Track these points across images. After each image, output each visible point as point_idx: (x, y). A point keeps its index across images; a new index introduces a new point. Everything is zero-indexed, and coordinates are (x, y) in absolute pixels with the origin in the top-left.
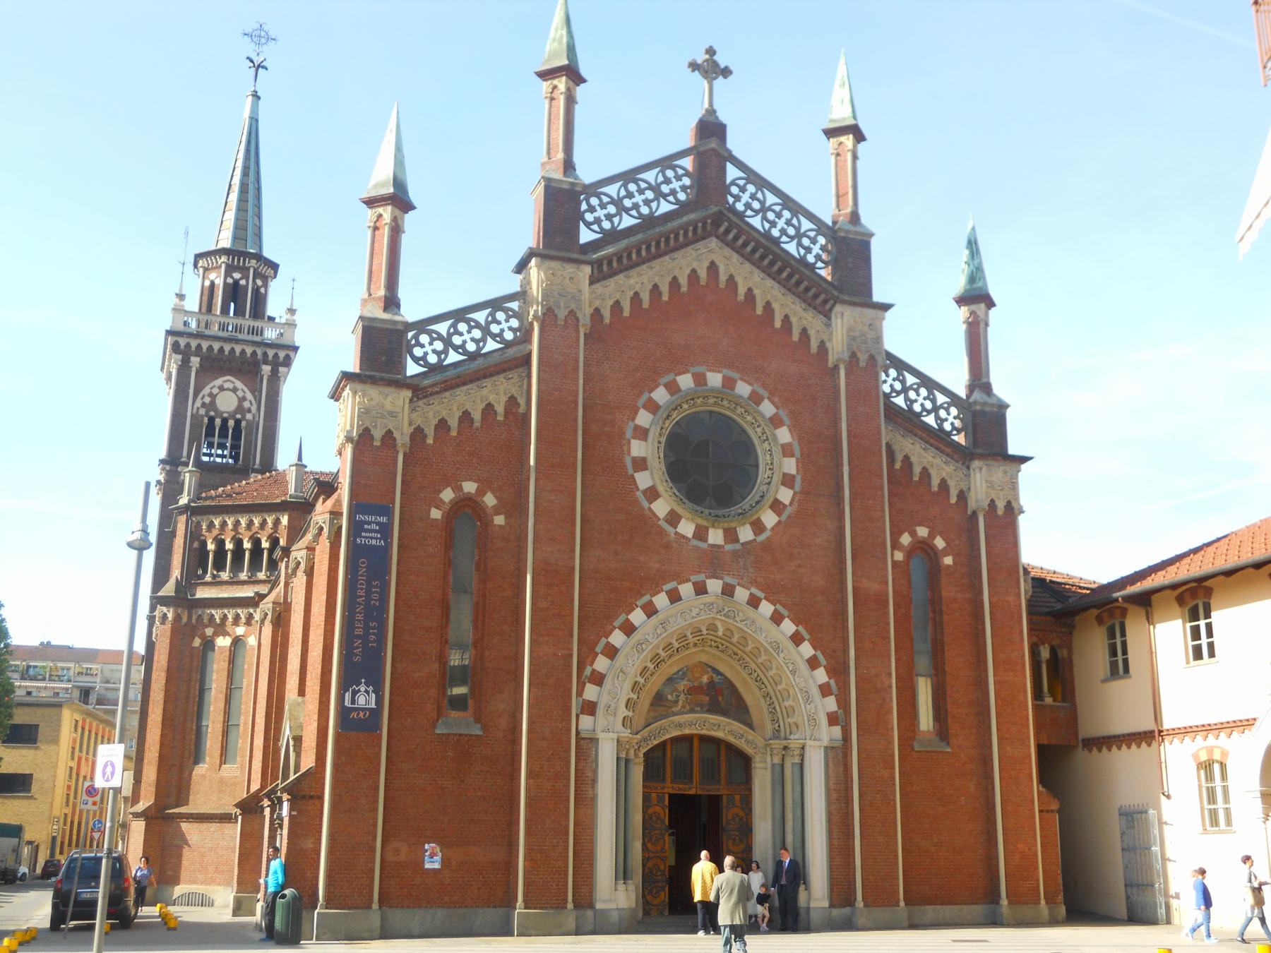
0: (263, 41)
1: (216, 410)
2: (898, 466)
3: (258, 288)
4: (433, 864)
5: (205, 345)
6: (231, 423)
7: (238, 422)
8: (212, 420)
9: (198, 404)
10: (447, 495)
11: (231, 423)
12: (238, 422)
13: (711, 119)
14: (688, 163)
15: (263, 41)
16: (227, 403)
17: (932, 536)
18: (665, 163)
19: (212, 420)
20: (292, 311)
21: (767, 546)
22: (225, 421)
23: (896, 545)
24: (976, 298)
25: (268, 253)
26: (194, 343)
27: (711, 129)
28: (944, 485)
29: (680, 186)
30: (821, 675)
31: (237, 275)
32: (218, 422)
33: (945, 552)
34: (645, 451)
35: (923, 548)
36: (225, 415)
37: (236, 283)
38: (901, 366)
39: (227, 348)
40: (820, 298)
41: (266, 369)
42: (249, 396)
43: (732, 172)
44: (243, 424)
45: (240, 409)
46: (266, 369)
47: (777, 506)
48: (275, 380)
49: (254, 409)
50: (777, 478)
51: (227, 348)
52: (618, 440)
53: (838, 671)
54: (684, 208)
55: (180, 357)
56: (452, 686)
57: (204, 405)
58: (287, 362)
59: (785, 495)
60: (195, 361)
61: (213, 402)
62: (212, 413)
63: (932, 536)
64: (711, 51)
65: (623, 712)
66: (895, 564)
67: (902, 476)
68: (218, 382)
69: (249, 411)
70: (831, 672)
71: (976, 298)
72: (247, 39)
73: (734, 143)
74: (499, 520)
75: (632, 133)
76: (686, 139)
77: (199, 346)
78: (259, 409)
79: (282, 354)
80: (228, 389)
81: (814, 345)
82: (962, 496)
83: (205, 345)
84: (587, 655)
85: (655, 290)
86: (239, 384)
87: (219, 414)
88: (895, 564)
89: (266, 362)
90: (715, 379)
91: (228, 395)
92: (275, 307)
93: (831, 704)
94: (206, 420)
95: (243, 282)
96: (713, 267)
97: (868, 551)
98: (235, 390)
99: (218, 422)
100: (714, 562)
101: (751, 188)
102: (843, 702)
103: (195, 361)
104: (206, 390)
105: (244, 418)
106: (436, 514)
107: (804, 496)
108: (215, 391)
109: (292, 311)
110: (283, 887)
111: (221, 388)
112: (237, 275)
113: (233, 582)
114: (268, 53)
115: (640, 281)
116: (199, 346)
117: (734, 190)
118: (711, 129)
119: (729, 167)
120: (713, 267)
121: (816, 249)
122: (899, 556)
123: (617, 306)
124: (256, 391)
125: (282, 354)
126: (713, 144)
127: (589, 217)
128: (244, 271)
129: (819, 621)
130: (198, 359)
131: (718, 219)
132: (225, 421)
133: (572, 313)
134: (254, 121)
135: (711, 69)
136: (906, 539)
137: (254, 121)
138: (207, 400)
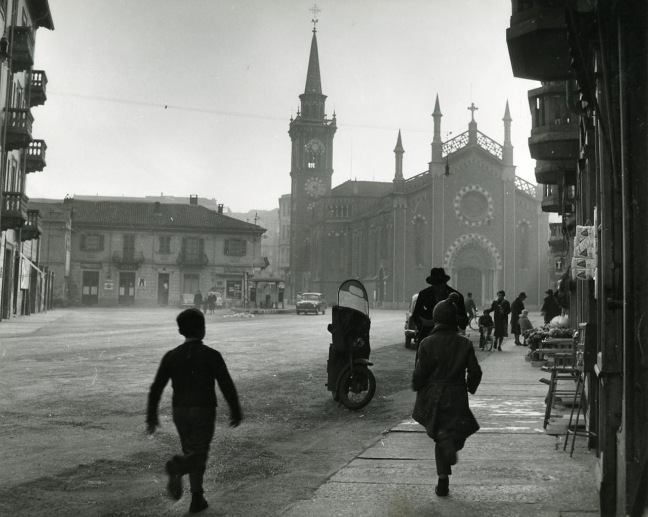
7: (319, 154)
14: (467, 134)
27: (473, 126)
29: (466, 140)
38: (520, 179)
43: (479, 135)
54: (467, 145)
56: (536, 428)
61: (311, 148)
64: (473, 104)
68: (312, 141)
72: (311, 11)
73: (479, 128)
75: (454, 129)
76: (466, 128)
84: (445, 252)
87: (313, 151)
90: (474, 224)
98: (317, 143)
101: (483, 138)
102: (503, 260)
109: (334, 115)
111: (313, 143)
114: (319, 16)
117: (479, 139)
118: (473, 126)
119: (478, 133)
121: (499, 152)
122: (518, 226)
127: (445, 150)
135: (473, 108)
136: (520, 222)
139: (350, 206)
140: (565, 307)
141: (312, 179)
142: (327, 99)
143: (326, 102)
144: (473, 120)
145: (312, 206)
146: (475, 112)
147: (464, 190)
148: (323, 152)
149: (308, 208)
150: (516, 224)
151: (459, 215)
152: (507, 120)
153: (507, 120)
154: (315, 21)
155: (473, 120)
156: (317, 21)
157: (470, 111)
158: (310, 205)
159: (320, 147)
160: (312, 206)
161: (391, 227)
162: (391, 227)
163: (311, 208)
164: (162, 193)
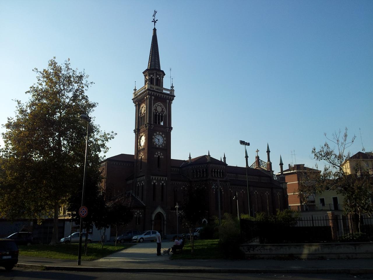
3: (158, 78)
24: (268, 152)
25: (161, 69)
31: (151, 76)
36: (159, 112)
37: (152, 77)
44: (163, 115)
45: (162, 111)
46: (168, 101)
48: (170, 104)
60: (153, 97)
62: (156, 112)
68: (157, 104)
71: (268, 152)
78: (166, 110)
80: (159, 106)
86: (162, 105)
91: (159, 107)
95: (153, 77)
98: (161, 106)
99: (158, 114)
108: (157, 106)
110: (276, 175)
111: (158, 105)
112: (151, 76)
130: (154, 97)
134: (155, 25)
137: (155, 25)
138: (155, 108)
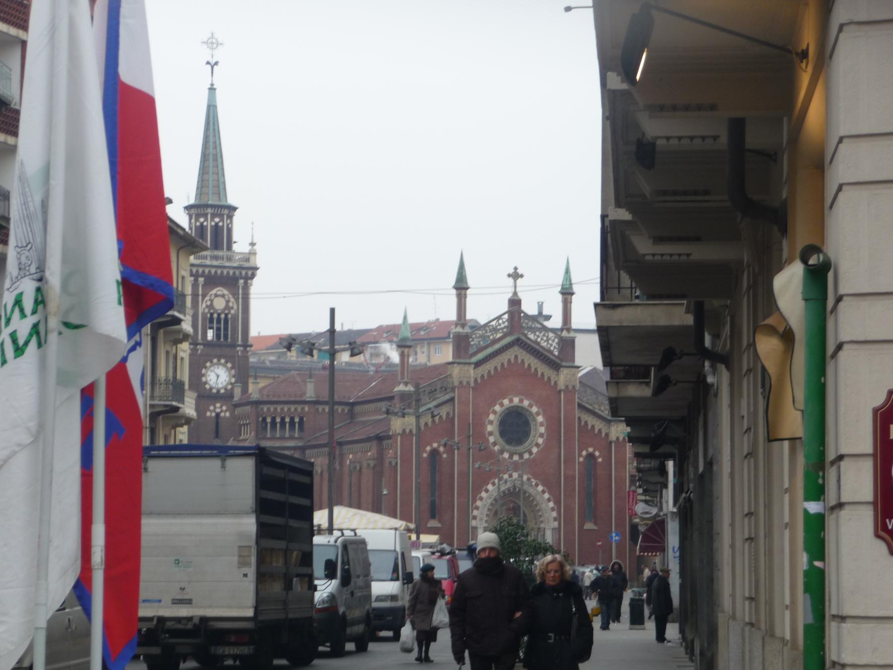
0: (215, 46)
1: (214, 308)
2: (583, 423)
4: (512, 560)
5: (207, 271)
6: (223, 316)
7: (226, 315)
8: (212, 315)
9: (204, 306)
10: (428, 448)
11: (223, 316)
12: (226, 315)
13: (516, 298)
14: (506, 316)
15: (215, 46)
16: (219, 304)
17: (594, 451)
18: (499, 318)
19: (212, 315)
20: (253, 244)
21: (534, 460)
22: (219, 315)
23: (580, 455)
26: (200, 270)
28: (600, 431)
30: (551, 504)
32: (215, 316)
33: (599, 457)
34: (492, 428)
35: (591, 456)
39: (219, 271)
40: (555, 366)
41: (241, 282)
42: (232, 300)
44: (229, 316)
45: (227, 307)
47: (537, 445)
48: (246, 287)
49: (235, 307)
50: (538, 435)
51: (219, 271)
52: (483, 426)
53: (558, 502)
55: (192, 278)
57: (207, 306)
58: (253, 276)
59: (540, 441)
60: (201, 280)
61: (212, 305)
63: (594, 451)
64: (516, 269)
65: (485, 518)
66: (579, 463)
67: (584, 429)
68: (214, 292)
69: (232, 308)
70: (555, 503)
74: (445, 456)
76: (504, 307)
77: (203, 271)
79: (250, 273)
81: (552, 383)
82: (607, 435)
83: (207, 271)
84: (474, 501)
85: (496, 368)
86: (226, 292)
87: (216, 311)
88: (579, 463)
89: (241, 278)
92: (240, 246)
93: (554, 514)
94: (209, 315)
96: (516, 357)
97: (570, 460)
98: (223, 296)
99: (215, 316)
100: (516, 467)
102: (559, 513)
103: (201, 280)
104: (207, 298)
105: (229, 313)
106: (425, 455)
107: (547, 442)
109: (253, 244)
111: (216, 296)
112: (217, 220)
113: (282, 438)
115: (489, 366)
116: (203, 271)
120: (516, 357)
121: (554, 344)
122: (581, 459)
123: (482, 376)
124: (235, 295)
125: (250, 273)
126: (516, 308)
128: (221, 216)
129: (552, 486)
131: (518, 340)
132: (219, 315)
133: (468, 382)
135: (516, 275)
136: (584, 453)
138: (209, 303)
139: (301, 419)
140: (171, 306)
141: (223, 361)
142: (237, 213)
143: (235, 219)
144: (515, 293)
145: (214, 411)
146: (519, 281)
147: (502, 405)
148: (233, 312)
149: (208, 414)
150: (580, 455)
151: (511, 457)
152: (567, 293)
153: (567, 293)
154: (213, 65)
155: (515, 293)
156: (216, 63)
157: (511, 280)
158: (212, 408)
159: (228, 302)
160: (214, 411)
161: (393, 463)
162: (393, 463)
163: (214, 414)
164: (223, 467)
